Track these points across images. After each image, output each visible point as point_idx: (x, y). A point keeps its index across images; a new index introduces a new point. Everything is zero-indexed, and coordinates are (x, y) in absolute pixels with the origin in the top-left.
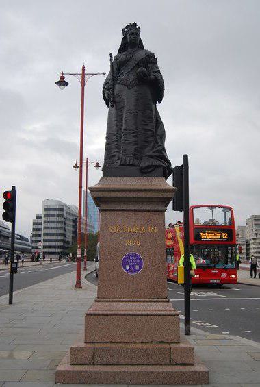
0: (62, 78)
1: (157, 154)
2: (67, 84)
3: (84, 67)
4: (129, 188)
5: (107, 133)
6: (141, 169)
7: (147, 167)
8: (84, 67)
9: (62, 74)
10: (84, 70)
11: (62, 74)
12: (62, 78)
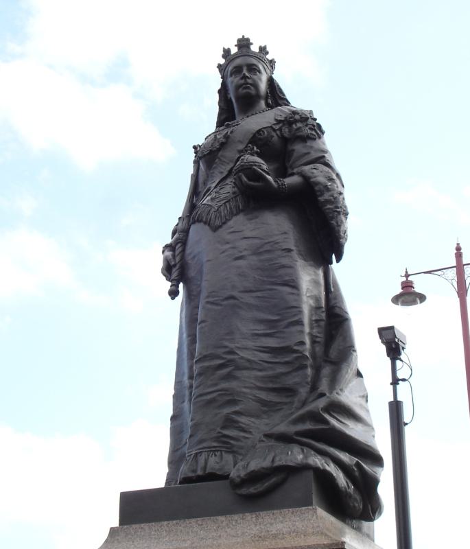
0: (407, 285)
1: (308, 426)
2: (422, 298)
3: (458, 249)
4: (315, 543)
5: (175, 389)
6: (237, 485)
7: (254, 477)
8: (458, 249)
9: (407, 275)
10: (459, 255)
11: (407, 275)
12: (407, 285)
